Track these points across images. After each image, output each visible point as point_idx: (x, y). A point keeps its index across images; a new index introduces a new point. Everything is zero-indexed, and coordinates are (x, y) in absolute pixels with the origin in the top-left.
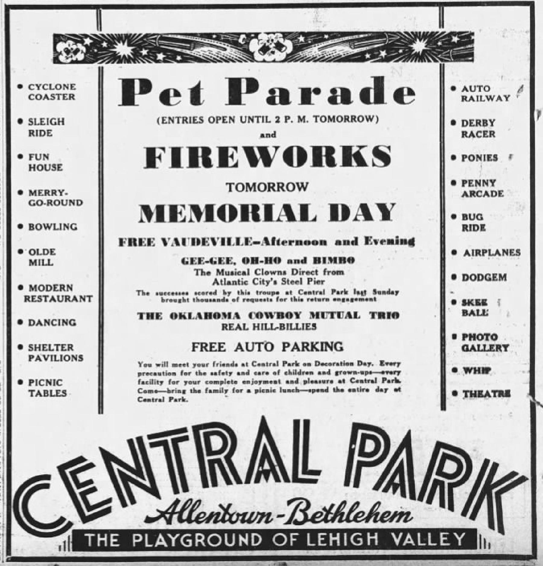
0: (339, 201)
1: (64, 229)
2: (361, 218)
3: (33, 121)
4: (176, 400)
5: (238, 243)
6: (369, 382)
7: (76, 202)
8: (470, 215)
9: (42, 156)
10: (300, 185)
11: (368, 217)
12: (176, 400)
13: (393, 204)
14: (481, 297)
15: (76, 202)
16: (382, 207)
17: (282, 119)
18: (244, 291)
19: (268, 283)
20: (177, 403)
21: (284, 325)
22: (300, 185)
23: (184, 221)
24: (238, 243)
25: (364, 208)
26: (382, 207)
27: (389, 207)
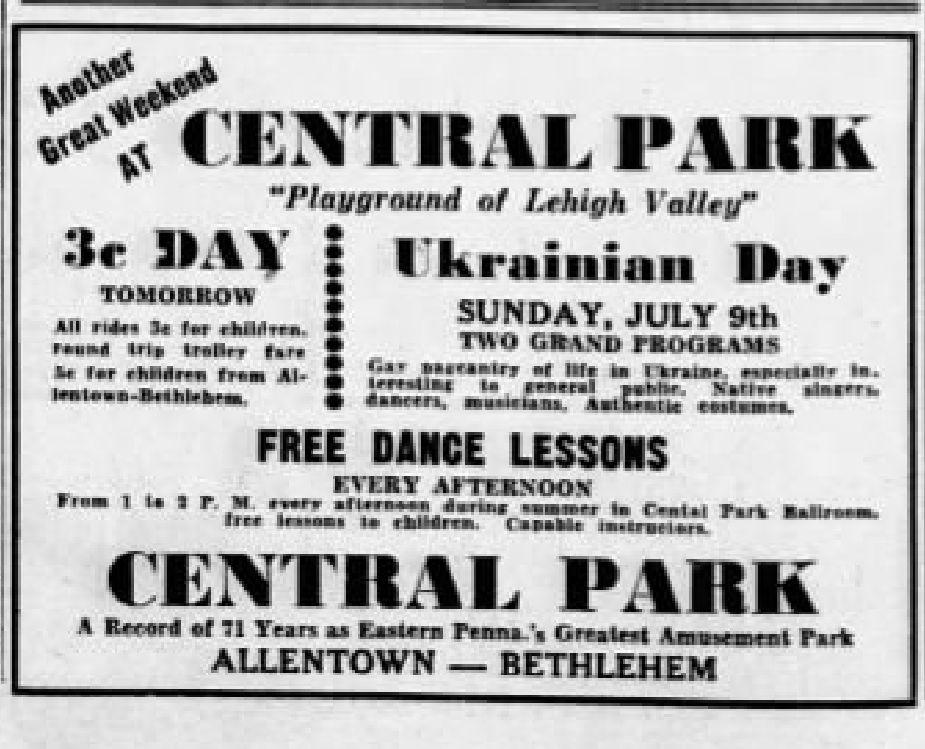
0: (174, 224)
1: (521, 304)
2: (217, 262)
3: (475, 308)
4: (822, 641)
5: (382, 128)
6: (572, 391)
7: (526, 310)
8: (481, 304)
9: (501, 309)
10: (387, 657)
11: (232, 260)
12: (822, 641)
13: (284, 234)
14: (813, 399)
15: (526, 310)
16: (262, 240)
17: (194, 502)
18: (577, 194)
19: (636, 139)
20: (827, 650)
21: (517, 658)
22: (387, 657)
23: (279, 160)
24: (382, 128)
25: (224, 240)
26: (262, 240)
27: (275, 238)
